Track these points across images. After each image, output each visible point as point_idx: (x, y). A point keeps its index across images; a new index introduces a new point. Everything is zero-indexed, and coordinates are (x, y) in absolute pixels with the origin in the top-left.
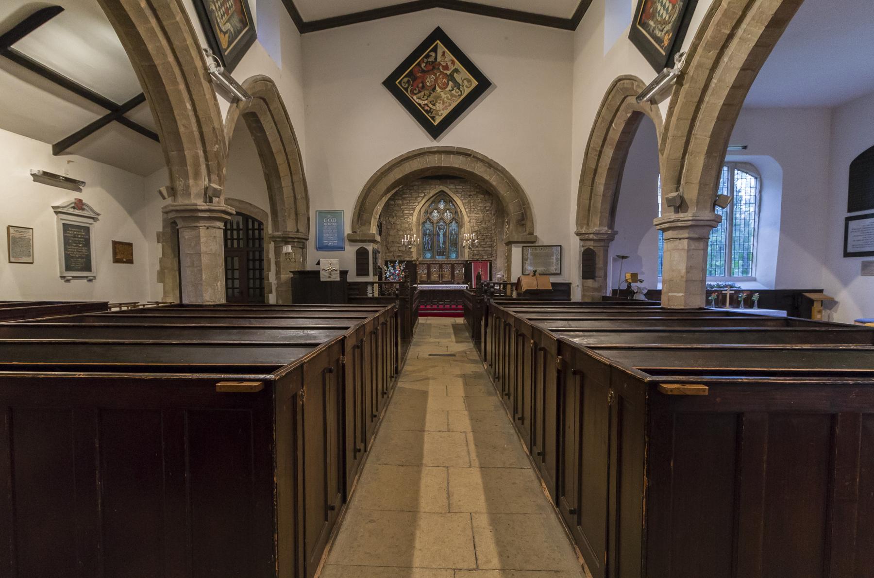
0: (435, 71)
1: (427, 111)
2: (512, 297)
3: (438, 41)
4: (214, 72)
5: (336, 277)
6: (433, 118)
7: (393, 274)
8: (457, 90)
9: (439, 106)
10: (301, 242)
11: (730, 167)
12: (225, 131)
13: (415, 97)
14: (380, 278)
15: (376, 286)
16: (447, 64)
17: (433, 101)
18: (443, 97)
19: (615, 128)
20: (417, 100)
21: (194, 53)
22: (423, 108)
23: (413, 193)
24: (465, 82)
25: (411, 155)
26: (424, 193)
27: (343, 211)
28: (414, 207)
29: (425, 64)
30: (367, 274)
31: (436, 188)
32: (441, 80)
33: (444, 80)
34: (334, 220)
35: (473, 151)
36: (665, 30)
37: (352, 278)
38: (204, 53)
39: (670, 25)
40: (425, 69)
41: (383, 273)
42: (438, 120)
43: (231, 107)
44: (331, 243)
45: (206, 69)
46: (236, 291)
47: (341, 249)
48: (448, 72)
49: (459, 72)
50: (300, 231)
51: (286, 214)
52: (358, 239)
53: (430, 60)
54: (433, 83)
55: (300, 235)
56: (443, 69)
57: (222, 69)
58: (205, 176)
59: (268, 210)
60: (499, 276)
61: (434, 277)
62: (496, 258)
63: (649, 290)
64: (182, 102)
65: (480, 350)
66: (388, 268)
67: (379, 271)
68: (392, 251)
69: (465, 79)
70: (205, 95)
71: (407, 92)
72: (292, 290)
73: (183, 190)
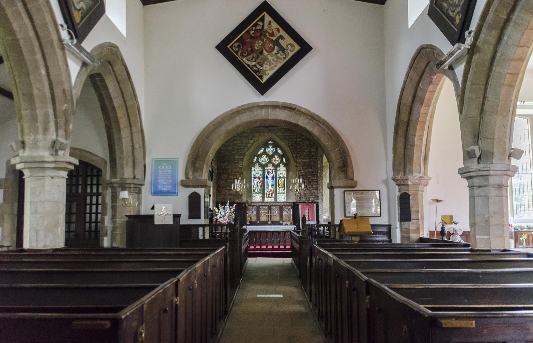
0: (263, 38)
1: (255, 71)
2: (336, 238)
3: (265, 13)
4: (68, 43)
5: (170, 221)
6: (261, 77)
7: (223, 216)
8: (282, 53)
9: (266, 67)
10: (137, 189)
11: (529, 119)
12: (74, 92)
13: (244, 59)
14: (211, 220)
15: (207, 229)
16: (273, 31)
17: (261, 63)
18: (270, 59)
19: (422, 87)
20: (247, 62)
21: (51, 28)
22: (252, 69)
23: (243, 140)
24: (289, 46)
25: (241, 109)
26: (254, 140)
27: (178, 159)
28: (244, 152)
29: (253, 32)
30: (199, 217)
31: (264, 135)
32: (268, 45)
33: (271, 45)
34: (169, 167)
35: (296, 105)
36: (456, 11)
37: (185, 221)
38: (60, 27)
39: (459, 8)
40: (253, 35)
41: (214, 215)
42: (265, 78)
43: (80, 70)
44: (165, 189)
45: (61, 41)
46: (72, 234)
47: (173, 193)
48: (274, 39)
49: (284, 38)
50: (137, 177)
51: (124, 162)
52: (191, 184)
53: (258, 28)
54: (260, 47)
55: (136, 181)
56: (269, 36)
57: (75, 41)
58: (53, 131)
59: (108, 159)
60: (325, 217)
61: (263, 218)
62: (322, 200)
63: (464, 232)
64: (37, 68)
65: (306, 290)
66: (219, 210)
67: (210, 214)
68: (222, 194)
69: (289, 44)
70: (58, 62)
71: (238, 55)
72: (127, 233)
73: (33, 143)
